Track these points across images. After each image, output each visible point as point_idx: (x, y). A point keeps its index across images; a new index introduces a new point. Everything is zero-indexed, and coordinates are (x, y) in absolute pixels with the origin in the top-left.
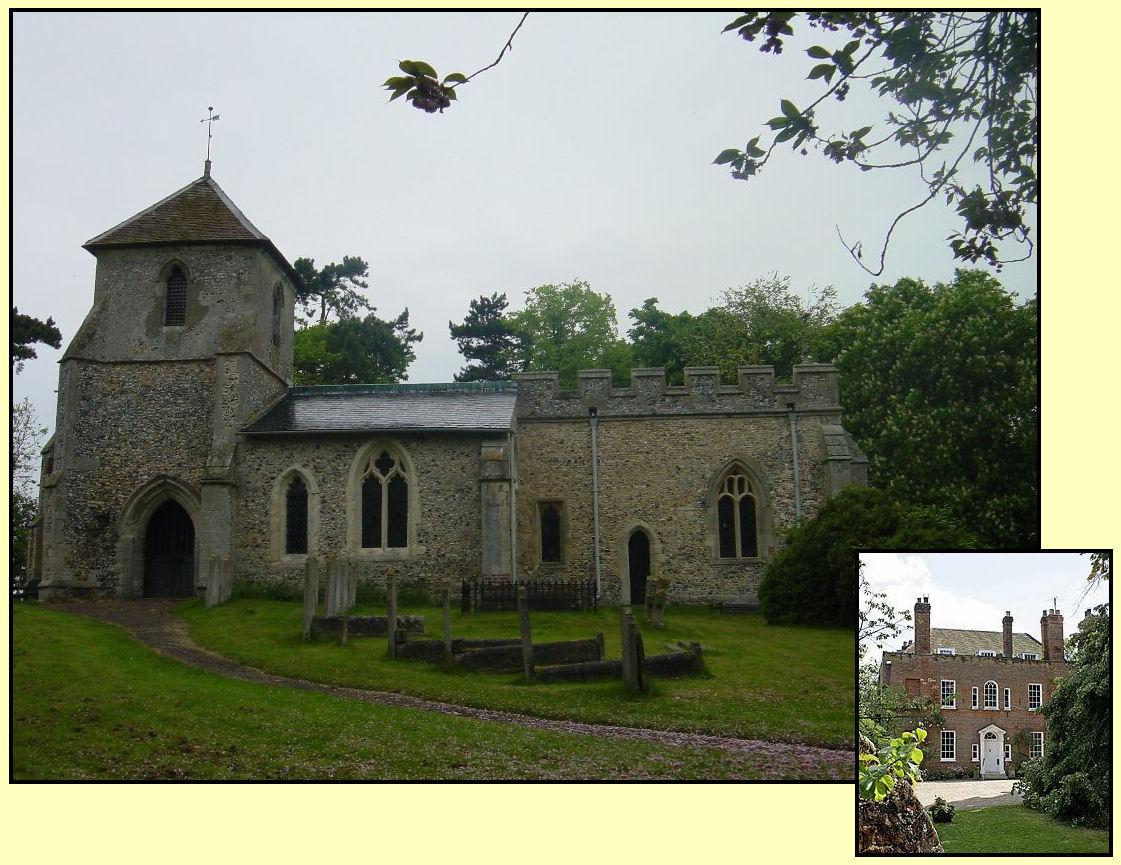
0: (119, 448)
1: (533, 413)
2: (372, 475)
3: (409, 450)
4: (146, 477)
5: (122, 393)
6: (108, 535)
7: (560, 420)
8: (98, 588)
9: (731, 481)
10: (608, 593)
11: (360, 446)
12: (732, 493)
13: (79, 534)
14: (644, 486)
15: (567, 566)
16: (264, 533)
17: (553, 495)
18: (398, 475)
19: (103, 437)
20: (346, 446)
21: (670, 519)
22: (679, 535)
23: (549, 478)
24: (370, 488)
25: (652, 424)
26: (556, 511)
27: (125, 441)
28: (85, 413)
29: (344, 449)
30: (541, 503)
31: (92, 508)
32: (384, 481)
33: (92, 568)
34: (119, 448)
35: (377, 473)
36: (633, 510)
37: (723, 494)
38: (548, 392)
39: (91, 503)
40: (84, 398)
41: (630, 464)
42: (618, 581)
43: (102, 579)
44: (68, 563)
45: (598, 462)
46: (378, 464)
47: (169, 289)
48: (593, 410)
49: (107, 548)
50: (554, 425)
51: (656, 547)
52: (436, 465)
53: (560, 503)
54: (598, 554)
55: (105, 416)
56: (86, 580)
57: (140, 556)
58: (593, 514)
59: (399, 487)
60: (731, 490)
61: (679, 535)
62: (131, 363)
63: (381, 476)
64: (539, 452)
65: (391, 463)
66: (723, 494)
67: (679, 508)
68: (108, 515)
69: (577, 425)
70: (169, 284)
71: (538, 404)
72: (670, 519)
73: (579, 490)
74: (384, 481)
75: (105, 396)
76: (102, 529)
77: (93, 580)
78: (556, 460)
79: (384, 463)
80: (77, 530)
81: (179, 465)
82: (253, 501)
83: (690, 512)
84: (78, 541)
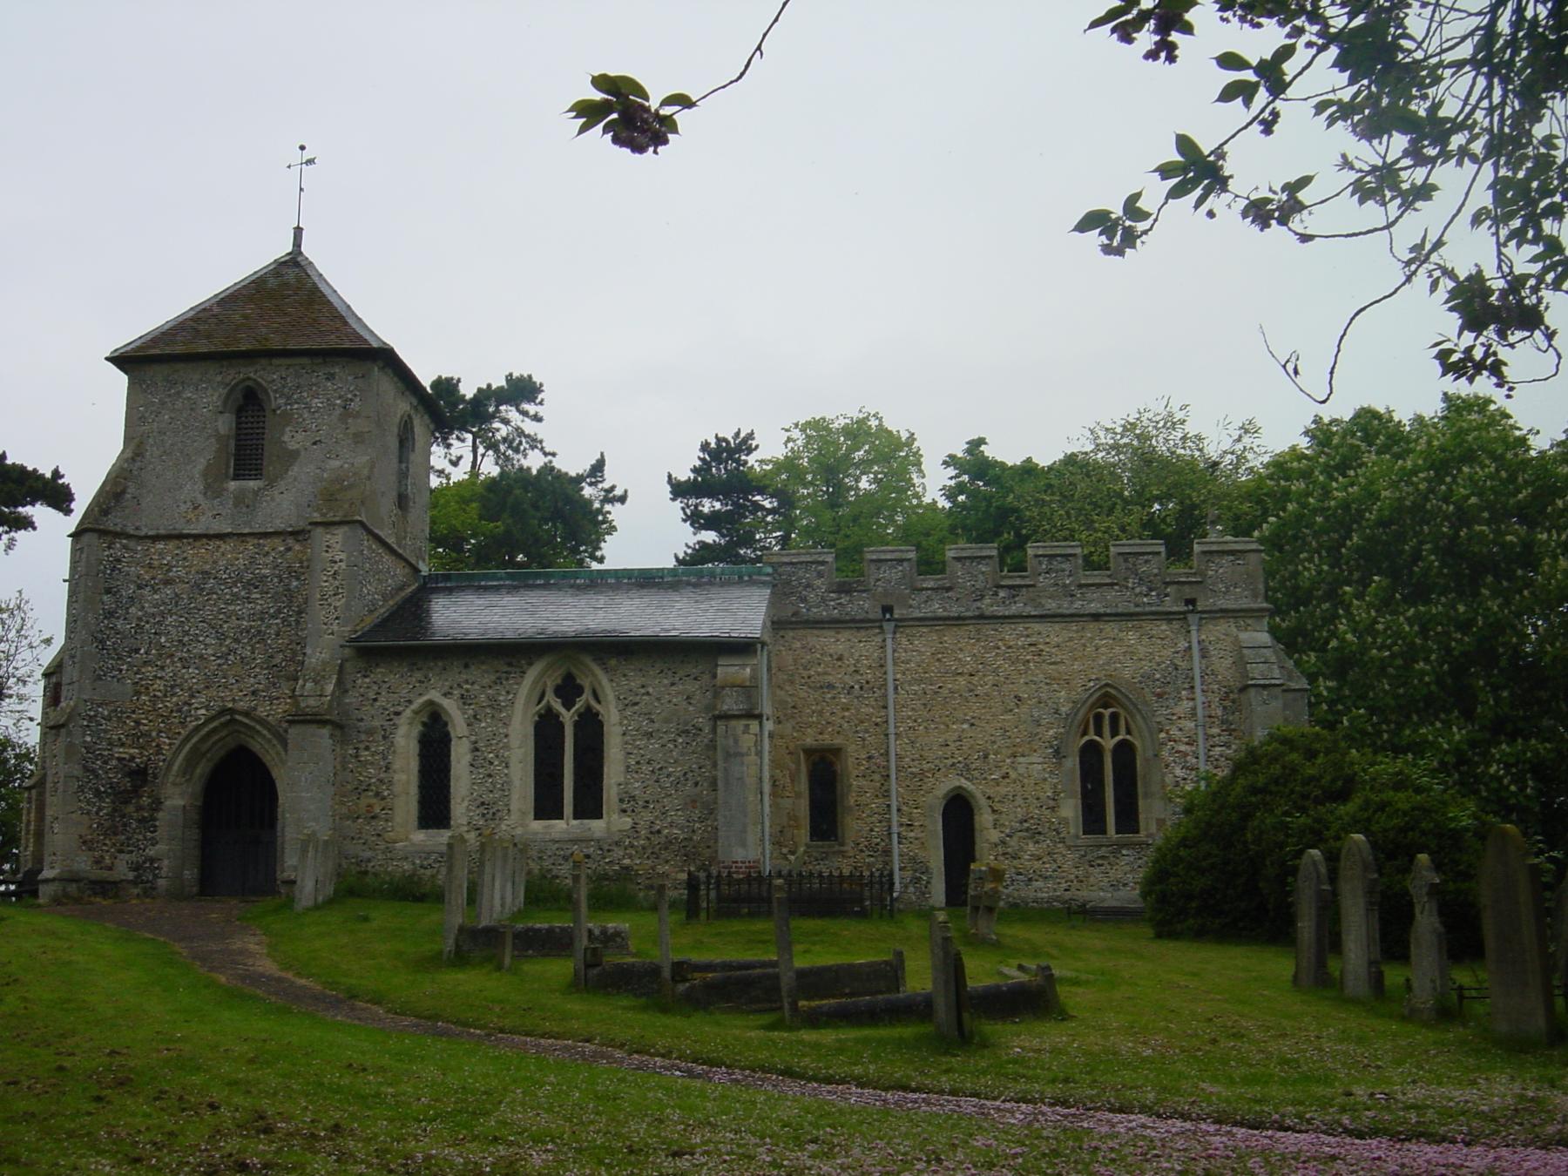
0: (162, 668)
1: (795, 614)
2: (549, 709)
3: (606, 670)
4: (203, 711)
5: (167, 582)
6: (145, 801)
7: (836, 624)
8: (129, 882)
9: (1098, 719)
10: (911, 889)
11: (530, 664)
12: (1100, 735)
13: (101, 800)
14: (965, 726)
15: (849, 848)
16: (384, 798)
17: (827, 739)
18: (589, 708)
19: (137, 651)
20: (510, 664)
21: (1006, 776)
22: (1019, 801)
23: (821, 713)
24: (547, 731)
25: (979, 632)
26: (831, 764)
27: (172, 655)
28: (110, 614)
29: (506, 668)
30: (809, 752)
31: (119, 759)
32: (568, 717)
33: (121, 851)
34: (162, 668)
35: (557, 706)
36: (949, 762)
37: (1086, 738)
38: (818, 582)
39: (119, 752)
40: (108, 591)
41: (945, 692)
42: (926, 871)
43: (136, 868)
44: (84, 843)
45: (896, 688)
46: (558, 691)
47: (238, 423)
48: (887, 609)
49: (142, 821)
50: (825, 632)
51: (984, 819)
52: (648, 694)
53: (837, 751)
54: (895, 829)
55: (140, 619)
56: (110, 869)
58: (887, 768)
59: (591, 727)
60: (1099, 733)
61: (1019, 801)
62: (180, 537)
63: (562, 710)
64: (805, 674)
65: (579, 691)
66: (1086, 738)
67: (1021, 759)
68: (146, 769)
69: (863, 633)
70: (238, 417)
71: (804, 600)
72: (1006, 776)
73: (867, 731)
74: (568, 717)
75: (140, 587)
76: (135, 792)
77: (122, 871)
78: (831, 686)
79: (569, 690)
80: (97, 793)
81: (254, 693)
82: (367, 748)
83: (1035, 764)
84: (100, 809)
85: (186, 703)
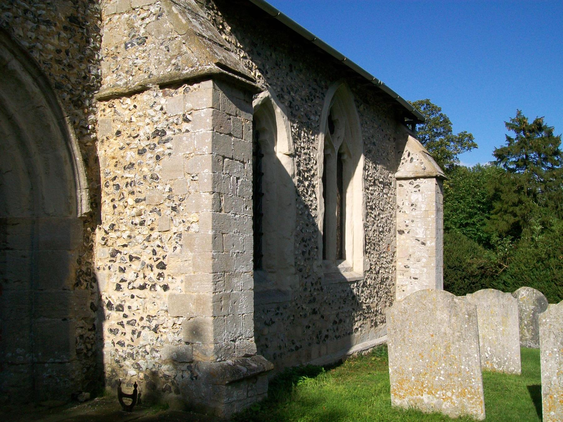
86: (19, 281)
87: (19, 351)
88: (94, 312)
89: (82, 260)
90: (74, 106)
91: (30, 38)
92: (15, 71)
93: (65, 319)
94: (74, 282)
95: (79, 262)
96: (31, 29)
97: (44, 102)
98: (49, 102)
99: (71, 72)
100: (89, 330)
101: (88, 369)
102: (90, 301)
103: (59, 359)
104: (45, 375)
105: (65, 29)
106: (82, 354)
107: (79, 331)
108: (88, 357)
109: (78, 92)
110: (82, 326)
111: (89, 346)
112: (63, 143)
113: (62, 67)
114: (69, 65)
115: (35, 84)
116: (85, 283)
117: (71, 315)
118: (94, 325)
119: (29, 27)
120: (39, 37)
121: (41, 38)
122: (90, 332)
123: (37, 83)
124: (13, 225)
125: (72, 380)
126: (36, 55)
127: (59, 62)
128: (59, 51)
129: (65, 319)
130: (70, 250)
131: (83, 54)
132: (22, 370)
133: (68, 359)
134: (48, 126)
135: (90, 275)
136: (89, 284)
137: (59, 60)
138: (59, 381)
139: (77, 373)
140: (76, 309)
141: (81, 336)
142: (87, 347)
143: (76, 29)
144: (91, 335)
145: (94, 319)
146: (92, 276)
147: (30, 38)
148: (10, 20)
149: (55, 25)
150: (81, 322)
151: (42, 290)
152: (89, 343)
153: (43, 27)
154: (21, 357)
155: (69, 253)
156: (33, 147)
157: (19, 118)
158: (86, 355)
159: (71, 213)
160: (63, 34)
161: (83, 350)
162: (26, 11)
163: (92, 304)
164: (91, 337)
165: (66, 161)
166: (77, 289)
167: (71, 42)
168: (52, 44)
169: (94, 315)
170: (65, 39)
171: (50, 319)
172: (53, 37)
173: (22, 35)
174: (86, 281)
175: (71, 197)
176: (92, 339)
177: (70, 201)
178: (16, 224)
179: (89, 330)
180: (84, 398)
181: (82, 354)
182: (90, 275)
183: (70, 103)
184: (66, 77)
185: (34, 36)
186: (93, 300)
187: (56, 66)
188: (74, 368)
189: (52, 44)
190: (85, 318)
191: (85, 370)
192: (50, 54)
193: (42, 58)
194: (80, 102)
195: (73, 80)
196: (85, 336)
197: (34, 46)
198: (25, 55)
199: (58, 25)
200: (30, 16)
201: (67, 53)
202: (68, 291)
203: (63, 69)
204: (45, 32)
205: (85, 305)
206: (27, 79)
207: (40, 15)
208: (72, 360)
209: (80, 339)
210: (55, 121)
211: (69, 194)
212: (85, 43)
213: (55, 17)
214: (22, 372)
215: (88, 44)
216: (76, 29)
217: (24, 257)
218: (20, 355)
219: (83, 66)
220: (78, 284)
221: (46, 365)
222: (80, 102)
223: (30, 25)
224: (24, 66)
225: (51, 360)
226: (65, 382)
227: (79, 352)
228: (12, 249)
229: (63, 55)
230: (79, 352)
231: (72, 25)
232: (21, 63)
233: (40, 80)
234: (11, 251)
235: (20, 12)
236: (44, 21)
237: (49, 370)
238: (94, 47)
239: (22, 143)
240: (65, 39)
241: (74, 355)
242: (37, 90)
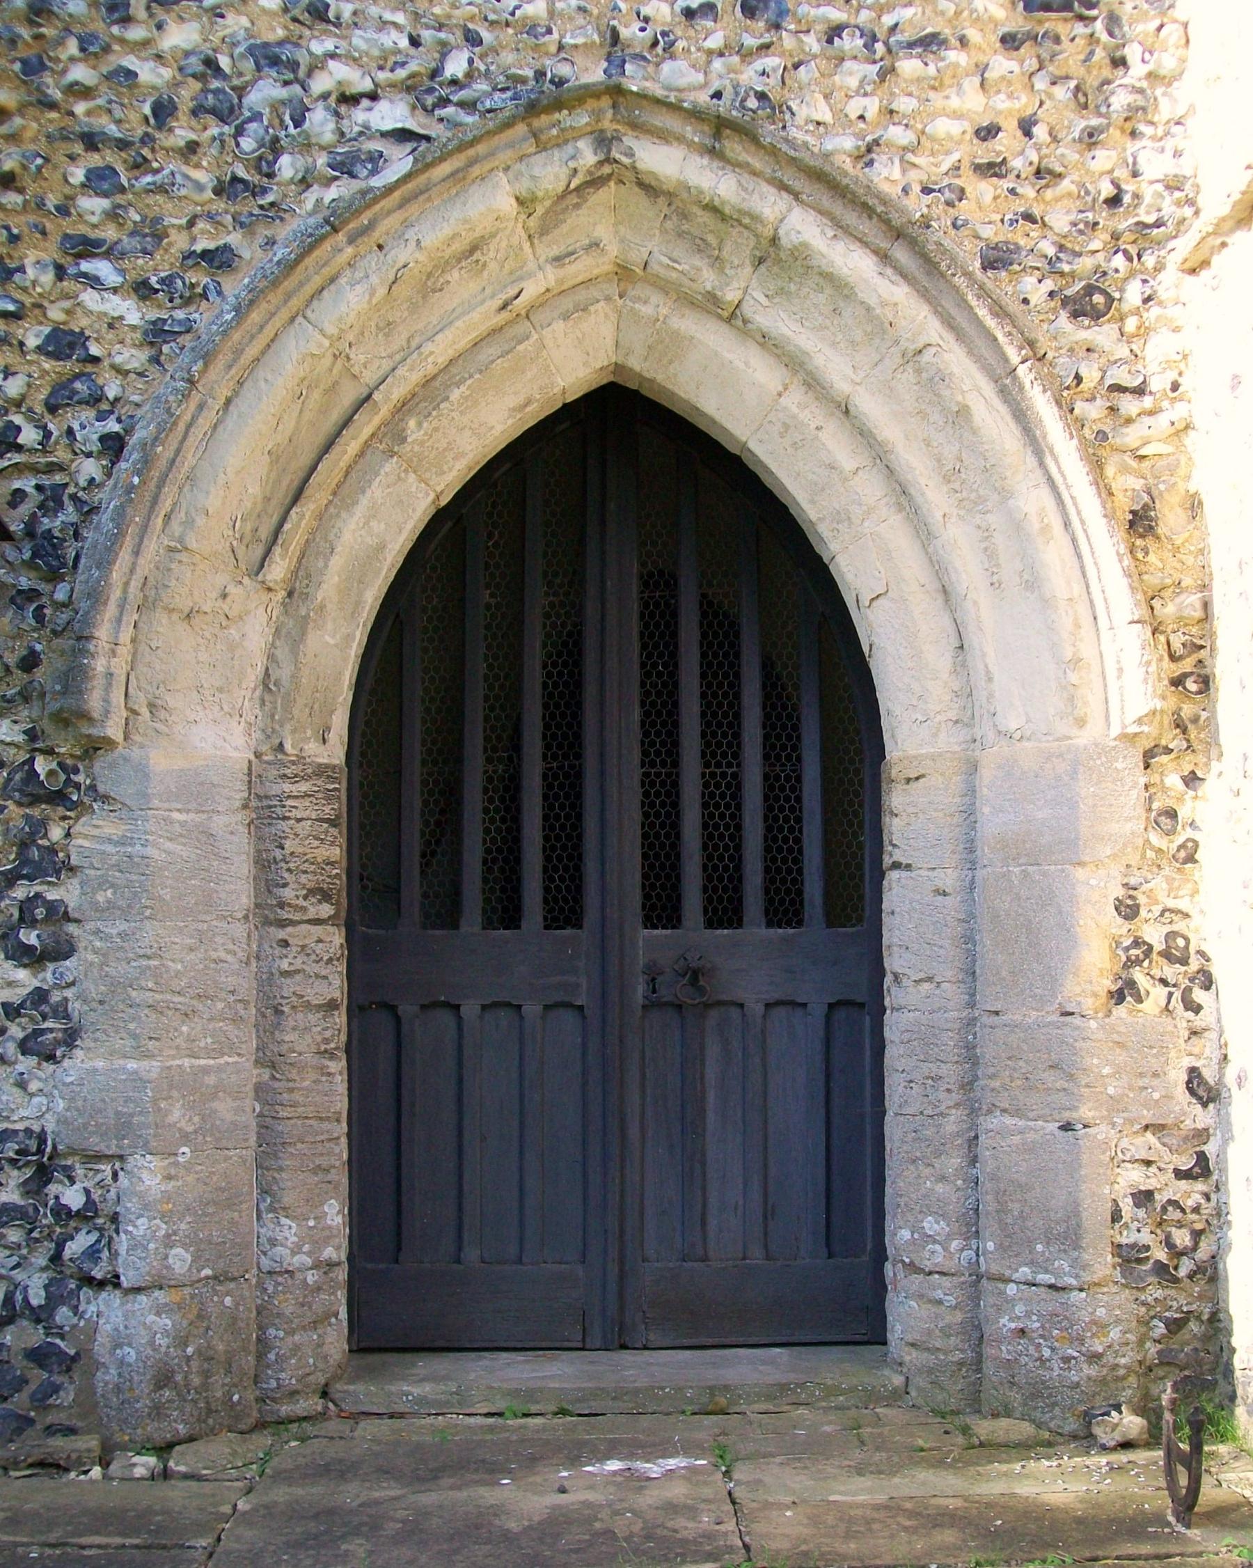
4: (391, 114)
57: (319, 959)
85: (268, 58)
86: (929, 979)
87: (931, 1225)
88: (1205, 1105)
89: (1142, 899)
90: (1075, 315)
91: (862, 117)
92: (805, 245)
93: (1067, 1127)
94: (1108, 984)
95: (1128, 910)
96: (861, 85)
97: (933, 330)
98: (949, 323)
99: (1049, 194)
100: (1180, 1174)
101: (1175, 1326)
102: (1187, 1062)
103: (1047, 1272)
104: (1007, 1323)
105: (1010, 42)
106: (1148, 1267)
107: (1134, 1177)
108: (1176, 1280)
109: (1087, 263)
110: (1143, 1155)
111: (1182, 1238)
112: (1031, 461)
113: (1006, 184)
114: (1038, 173)
115: (889, 271)
116: (1160, 992)
117: (1086, 1112)
118: (1202, 1158)
119: (853, 82)
120: (894, 106)
121: (904, 104)
122: (1184, 1185)
123: (895, 268)
124: (908, 780)
125: (1094, 1357)
126: (886, 175)
127: (993, 170)
128: (988, 133)
129: (1067, 1127)
130: (1081, 864)
131: (1100, 115)
132: (939, 1294)
133: (1077, 1277)
134: (963, 413)
135: (1184, 961)
136: (1177, 995)
137: (991, 165)
138: (1047, 1353)
139: (1115, 1334)
140: (1111, 1090)
141: (1144, 1198)
142: (1169, 1243)
143: (1062, 29)
144: (1191, 1193)
145: (1202, 1135)
146: (1195, 964)
147: (862, 117)
148: (770, 85)
149: (963, 42)
150: (1139, 1140)
151: (997, 1013)
152: (1180, 1225)
153: (909, 66)
154: (938, 1247)
155: (1080, 873)
156: (935, 498)
157: (869, 406)
158: (1161, 1269)
159: (1081, 722)
160: (1002, 65)
161: (1147, 1248)
162: (835, 32)
163: (1193, 1072)
164: (1190, 1203)
165: (1045, 529)
166: (1121, 1011)
167: (1041, 83)
168: (957, 115)
169: (1201, 1117)
170: (1010, 83)
171: (1021, 1123)
172: (960, 85)
173: (827, 117)
174: (1164, 982)
175: (1076, 662)
176: (1196, 1210)
177: (1073, 678)
178: (917, 778)
179: (1180, 1174)
180: (1118, 1437)
181: (1148, 1267)
182: (1184, 961)
183: (1054, 310)
184: (1029, 217)
185: (872, 106)
186: (1198, 1057)
187: (983, 190)
188: (1101, 1312)
189: (957, 115)
190: (1162, 1127)
191: (1160, 1329)
192: (948, 153)
193: (914, 175)
194: (1098, 299)
195: (1060, 221)
196: (1161, 1198)
197: (876, 142)
198: (833, 190)
199: (973, 35)
200: (850, 43)
201: (1026, 128)
202: (1076, 1020)
203: (1012, 191)
204: (919, 80)
205: (1155, 1075)
206: (854, 262)
207: (894, 28)
208: (1098, 1285)
209: (1137, 1205)
210: (988, 389)
211: (1068, 654)
212: (1106, 72)
213: (958, 14)
214: (940, 1302)
215: (1120, 71)
216: (1062, 29)
217: (945, 894)
218: (935, 1242)
219: (1103, 159)
220: (1124, 992)
221: (1011, 1289)
222: (1098, 299)
223: (855, 73)
224: (837, 224)
225: (1025, 1272)
226: (1067, 1360)
227: (1130, 1257)
228: (908, 867)
229: (1007, 143)
230: (1130, 1257)
231: (1040, 22)
232: (821, 212)
233: (901, 254)
234: (904, 874)
235: (812, 43)
236: (911, 45)
237: (1019, 1309)
238: (1151, 76)
239: (902, 494)
240: (1010, 83)
241: (1103, 1265)
242: (900, 293)
